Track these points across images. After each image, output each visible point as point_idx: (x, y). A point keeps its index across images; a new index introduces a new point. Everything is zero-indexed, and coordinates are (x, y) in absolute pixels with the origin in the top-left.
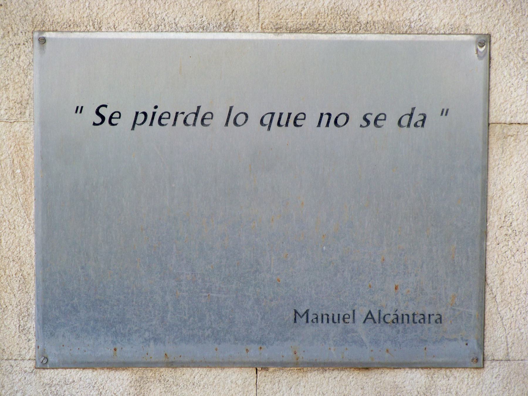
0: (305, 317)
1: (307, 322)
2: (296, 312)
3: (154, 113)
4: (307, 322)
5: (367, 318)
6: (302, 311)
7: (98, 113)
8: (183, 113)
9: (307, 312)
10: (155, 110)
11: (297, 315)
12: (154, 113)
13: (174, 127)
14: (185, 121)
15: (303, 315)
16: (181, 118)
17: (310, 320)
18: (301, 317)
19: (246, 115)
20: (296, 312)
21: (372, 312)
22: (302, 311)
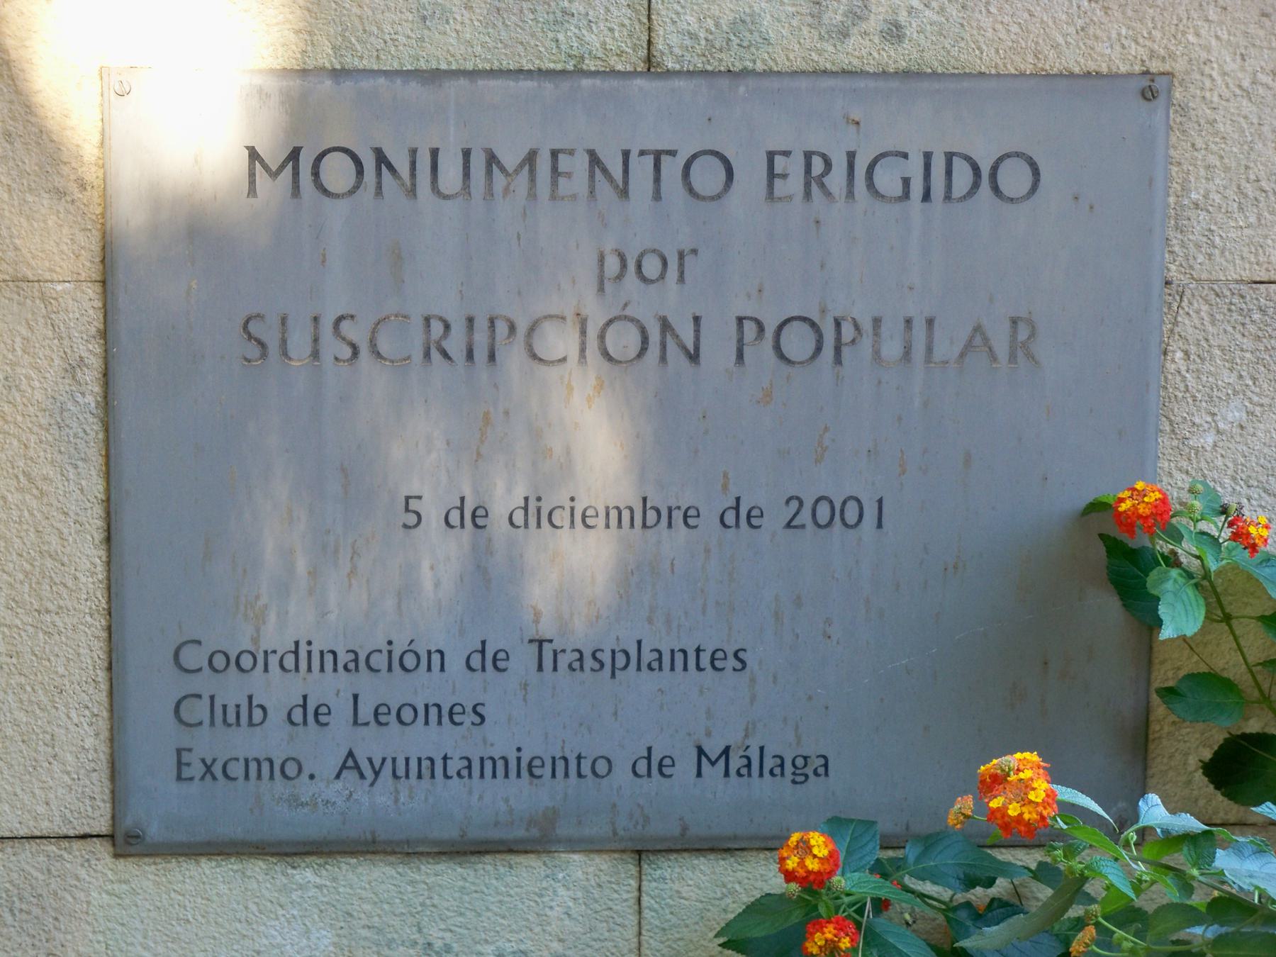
0: (722, 762)
1: (727, 774)
2: (701, 752)
3: (519, 759)
4: (727, 774)
5: (344, 767)
6: (714, 750)
7: (482, 718)
8: (275, 652)
9: (726, 751)
10: (309, 648)
11: (704, 759)
12: (519, 759)
13: (247, 693)
14: (282, 667)
15: (717, 760)
16: (274, 660)
17: (733, 771)
18: (713, 763)
19: (609, 761)
20: (701, 752)
21: (356, 752)
22: (714, 750)
